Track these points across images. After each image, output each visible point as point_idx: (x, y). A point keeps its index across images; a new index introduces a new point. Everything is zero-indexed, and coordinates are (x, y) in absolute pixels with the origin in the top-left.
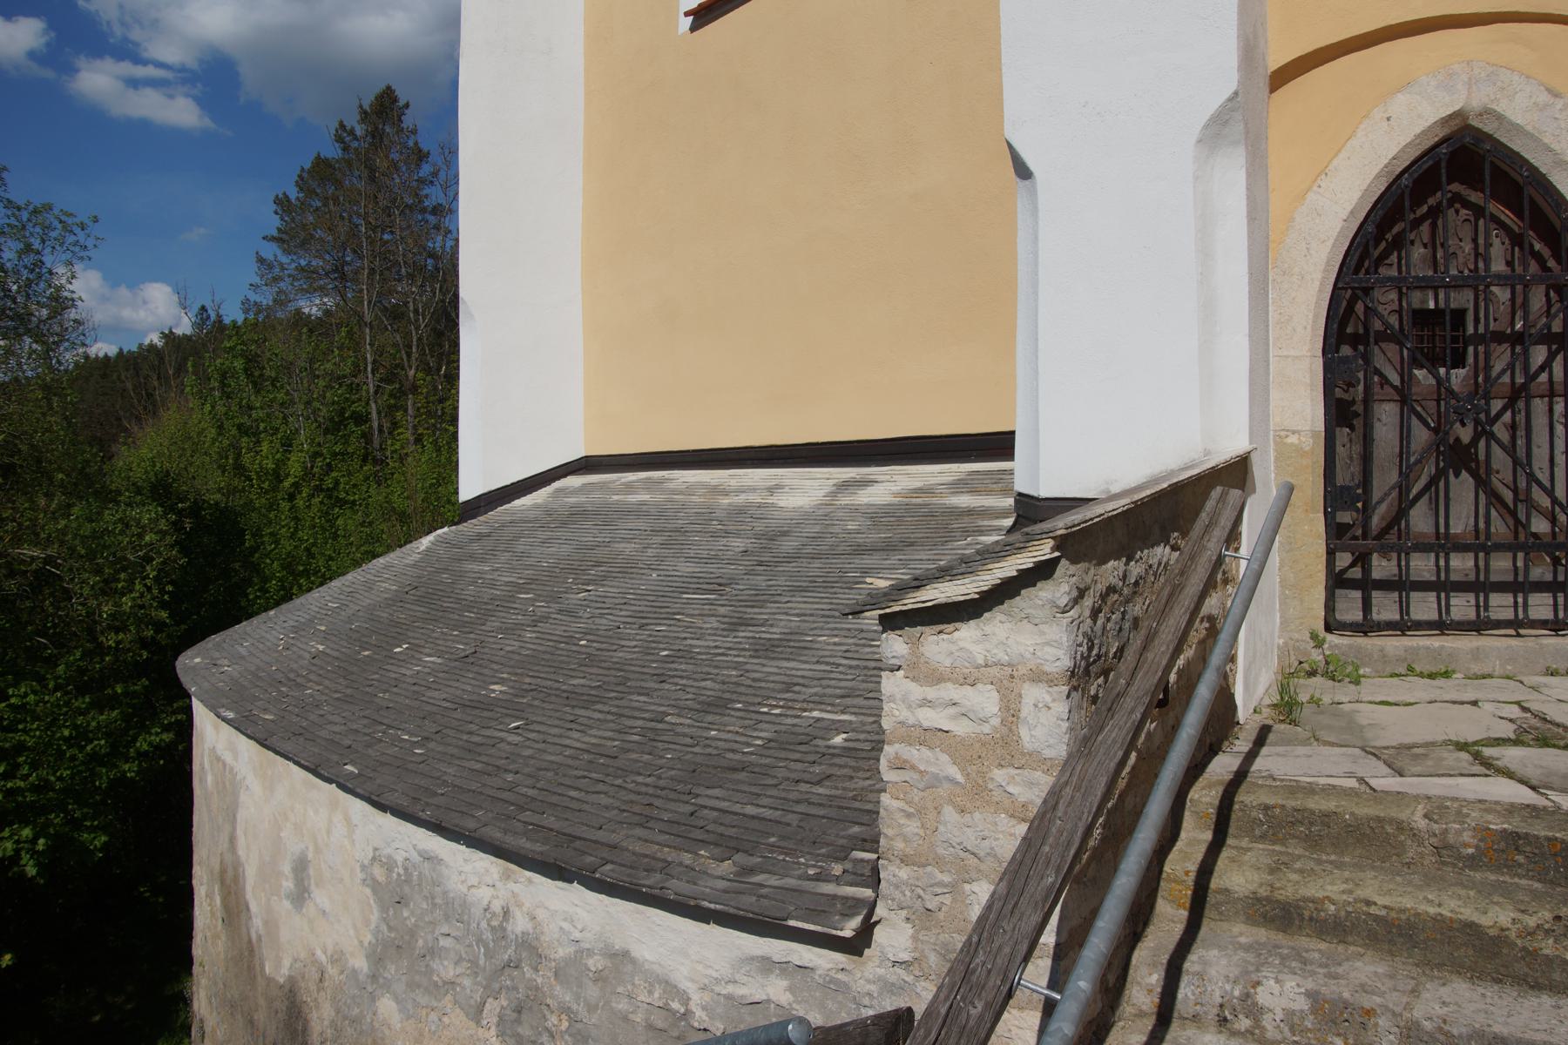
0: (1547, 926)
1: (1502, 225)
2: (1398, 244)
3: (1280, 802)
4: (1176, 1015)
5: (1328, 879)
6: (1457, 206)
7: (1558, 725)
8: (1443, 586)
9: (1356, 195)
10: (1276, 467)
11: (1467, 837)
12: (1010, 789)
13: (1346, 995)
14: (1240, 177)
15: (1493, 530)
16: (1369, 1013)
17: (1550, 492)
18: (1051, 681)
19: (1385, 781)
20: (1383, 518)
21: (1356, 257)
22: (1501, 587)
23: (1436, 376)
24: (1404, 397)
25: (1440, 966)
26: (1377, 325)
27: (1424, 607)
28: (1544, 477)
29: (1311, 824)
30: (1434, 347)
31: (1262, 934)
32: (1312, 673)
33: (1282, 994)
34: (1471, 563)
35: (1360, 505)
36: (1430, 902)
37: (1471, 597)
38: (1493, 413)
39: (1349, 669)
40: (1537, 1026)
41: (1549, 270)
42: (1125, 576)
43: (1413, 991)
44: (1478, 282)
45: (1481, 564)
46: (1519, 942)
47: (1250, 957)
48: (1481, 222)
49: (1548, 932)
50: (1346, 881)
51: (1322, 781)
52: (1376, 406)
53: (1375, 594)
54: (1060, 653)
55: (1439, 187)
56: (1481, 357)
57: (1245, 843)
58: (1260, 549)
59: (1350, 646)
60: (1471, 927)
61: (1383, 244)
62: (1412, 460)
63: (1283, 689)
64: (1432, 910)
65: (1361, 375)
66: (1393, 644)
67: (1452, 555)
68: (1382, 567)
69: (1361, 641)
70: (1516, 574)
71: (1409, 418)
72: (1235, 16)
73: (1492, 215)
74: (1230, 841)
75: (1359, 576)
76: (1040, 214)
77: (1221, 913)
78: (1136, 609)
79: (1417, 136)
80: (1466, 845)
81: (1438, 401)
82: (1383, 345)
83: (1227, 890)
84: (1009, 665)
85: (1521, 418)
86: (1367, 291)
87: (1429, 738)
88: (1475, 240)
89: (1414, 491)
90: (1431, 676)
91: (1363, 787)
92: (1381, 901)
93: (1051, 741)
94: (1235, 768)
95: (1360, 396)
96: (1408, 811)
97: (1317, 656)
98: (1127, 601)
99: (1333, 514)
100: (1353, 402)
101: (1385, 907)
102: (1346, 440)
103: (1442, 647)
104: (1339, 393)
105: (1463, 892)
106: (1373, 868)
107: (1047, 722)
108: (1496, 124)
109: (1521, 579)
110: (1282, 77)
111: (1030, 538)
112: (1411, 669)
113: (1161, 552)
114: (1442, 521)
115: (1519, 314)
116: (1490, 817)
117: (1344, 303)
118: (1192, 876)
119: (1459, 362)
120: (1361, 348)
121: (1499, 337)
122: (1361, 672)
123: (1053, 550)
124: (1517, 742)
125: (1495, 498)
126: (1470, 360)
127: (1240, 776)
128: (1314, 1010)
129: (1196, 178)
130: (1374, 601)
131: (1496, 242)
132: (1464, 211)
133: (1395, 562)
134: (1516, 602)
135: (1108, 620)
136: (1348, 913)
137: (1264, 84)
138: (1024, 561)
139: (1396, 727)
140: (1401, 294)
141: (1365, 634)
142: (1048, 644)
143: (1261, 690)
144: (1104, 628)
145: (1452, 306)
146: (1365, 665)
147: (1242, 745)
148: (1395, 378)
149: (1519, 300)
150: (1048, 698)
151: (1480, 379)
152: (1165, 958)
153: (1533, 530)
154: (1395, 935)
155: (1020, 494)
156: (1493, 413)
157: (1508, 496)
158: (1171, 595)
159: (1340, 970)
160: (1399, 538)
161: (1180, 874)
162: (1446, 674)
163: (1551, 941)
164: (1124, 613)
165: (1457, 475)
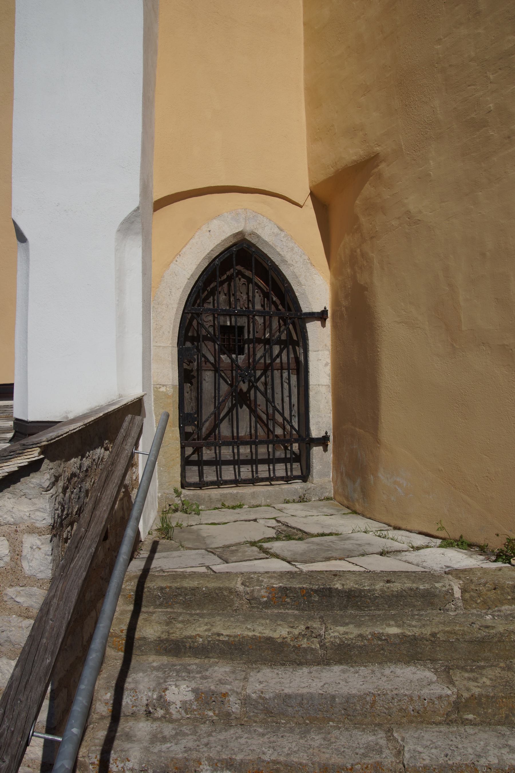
0: (303, 633)
1: (259, 288)
2: (212, 293)
3: (169, 585)
4: (122, 714)
5: (197, 624)
6: (240, 276)
7: (294, 528)
8: (237, 462)
9: (194, 267)
10: (155, 404)
11: (263, 592)
12: (18, 599)
13: (213, 687)
15: (258, 434)
16: (225, 695)
17: (282, 415)
18: (40, 533)
19: (220, 567)
20: (207, 429)
21: (194, 298)
22: (263, 462)
23: (231, 358)
24: (216, 369)
25: (256, 662)
26: (204, 332)
27: (228, 473)
28: (279, 408)
29: (186, 595)
30: (230, 344)
31: (165, 659)
32: (176, 511)
33: (179, 693)
34: (249, 450)
35: (196, 423)
36: (249, 629)
37: (249, 467)
38: (257, 377)
39: (194, 507)
40: (303, 685)
41: (280, 310)
42: (80, 467)
43: (245, 678)
44: (249, 314)
45: (254, 451)
46: (291, 643)
47: (160, 674)
48: (251, 285)
49: (304, 636)
50: (206, 624)
51: (189, 570)
52: (203, 372)
53: (205, 468)
54: (45, 515)
55: (232, 267)
56: (251, 350)
57: (151, 609)
58: (154, 449)
59: (194, 495)
60: (269, 639)
61: (206, 293)
62: (221, 399)
63: (163, 520)
64: (250, 634)
65: (196, 357)
66: (215, 493)
67: (240, 447)
68: (208, 454)
69: (199, 492)
70: (269, 455)
71: (219, 379)
73: (256, 283)
74: (143, 609)
75: (197, 459)
77: (142, 651)
78: (87, 485)
79: (223, 241)
80: (263, 597)
81: (232, 371)
82: (206, 342)
83: (144, 638)
84: (14, 524)
85: (269, 379)
86: (199, 315)
87: (237, 541)
88: (248, 294)
89: (222, 416)
90: (233, 508)
91: (209, 571)
92: (225, 633)
93: (42, 568)
94: (142, 567)
95: (195, 368)
96: (234, 583)
97: (178, 501)
98: (82, 481)
99: (183, 427)
100: (192, 371)
101: (227, 636)
102: (189, 390)
103: (238, 493)
104: (185, 366)
105: (263, 622)
106: (219, 615)
107: (39, 557)
108: (257, 240)
109: (271, 457)
110: (160, 204)
111: (26, 447)
112: (223, 505)
113: (100, 451)
114: (235, 430)
115: (267, 330)
116: (273, 581)
117: (188, 321)
118: (125, 632)
119: (241, 352)
120: (196, 343)
121: (259, 341)
122: (200, 508)
123: (40, 454)
124: (277, 539)
125: (259, 418)
126: (246, 351)
127: (146, 571)
128: (197, 699)
130: (204, 471)
131: (257, 295)
132: (242, 280)
133: (213, 451)
134: (269, 469)
135: (72, 492)
136: (209, 641)
138: (22, 461)
139: (223, 535)
140: (214, 318)
141: (201, 488)
142: (37, 510)
143: (151, 521)
144: (70, 498)
145: (238, 325)
146: (201, 504)
147: (144, 554)
148: (212, 359)
149: (267, 323)
150: (39, 543)
151: (251, 361)
152: (113, 683)
153: (276, 434)
154: (235, 650)
155: (17, 419)
156: (257, 377)
157: (264, 417)
158: (107, 477)
159: (207, 673)
160: (215, 439)
161: (118, 632)
162: (240, 506)
163: (305, 640)
164: (80, 488)
165: (241, 407)
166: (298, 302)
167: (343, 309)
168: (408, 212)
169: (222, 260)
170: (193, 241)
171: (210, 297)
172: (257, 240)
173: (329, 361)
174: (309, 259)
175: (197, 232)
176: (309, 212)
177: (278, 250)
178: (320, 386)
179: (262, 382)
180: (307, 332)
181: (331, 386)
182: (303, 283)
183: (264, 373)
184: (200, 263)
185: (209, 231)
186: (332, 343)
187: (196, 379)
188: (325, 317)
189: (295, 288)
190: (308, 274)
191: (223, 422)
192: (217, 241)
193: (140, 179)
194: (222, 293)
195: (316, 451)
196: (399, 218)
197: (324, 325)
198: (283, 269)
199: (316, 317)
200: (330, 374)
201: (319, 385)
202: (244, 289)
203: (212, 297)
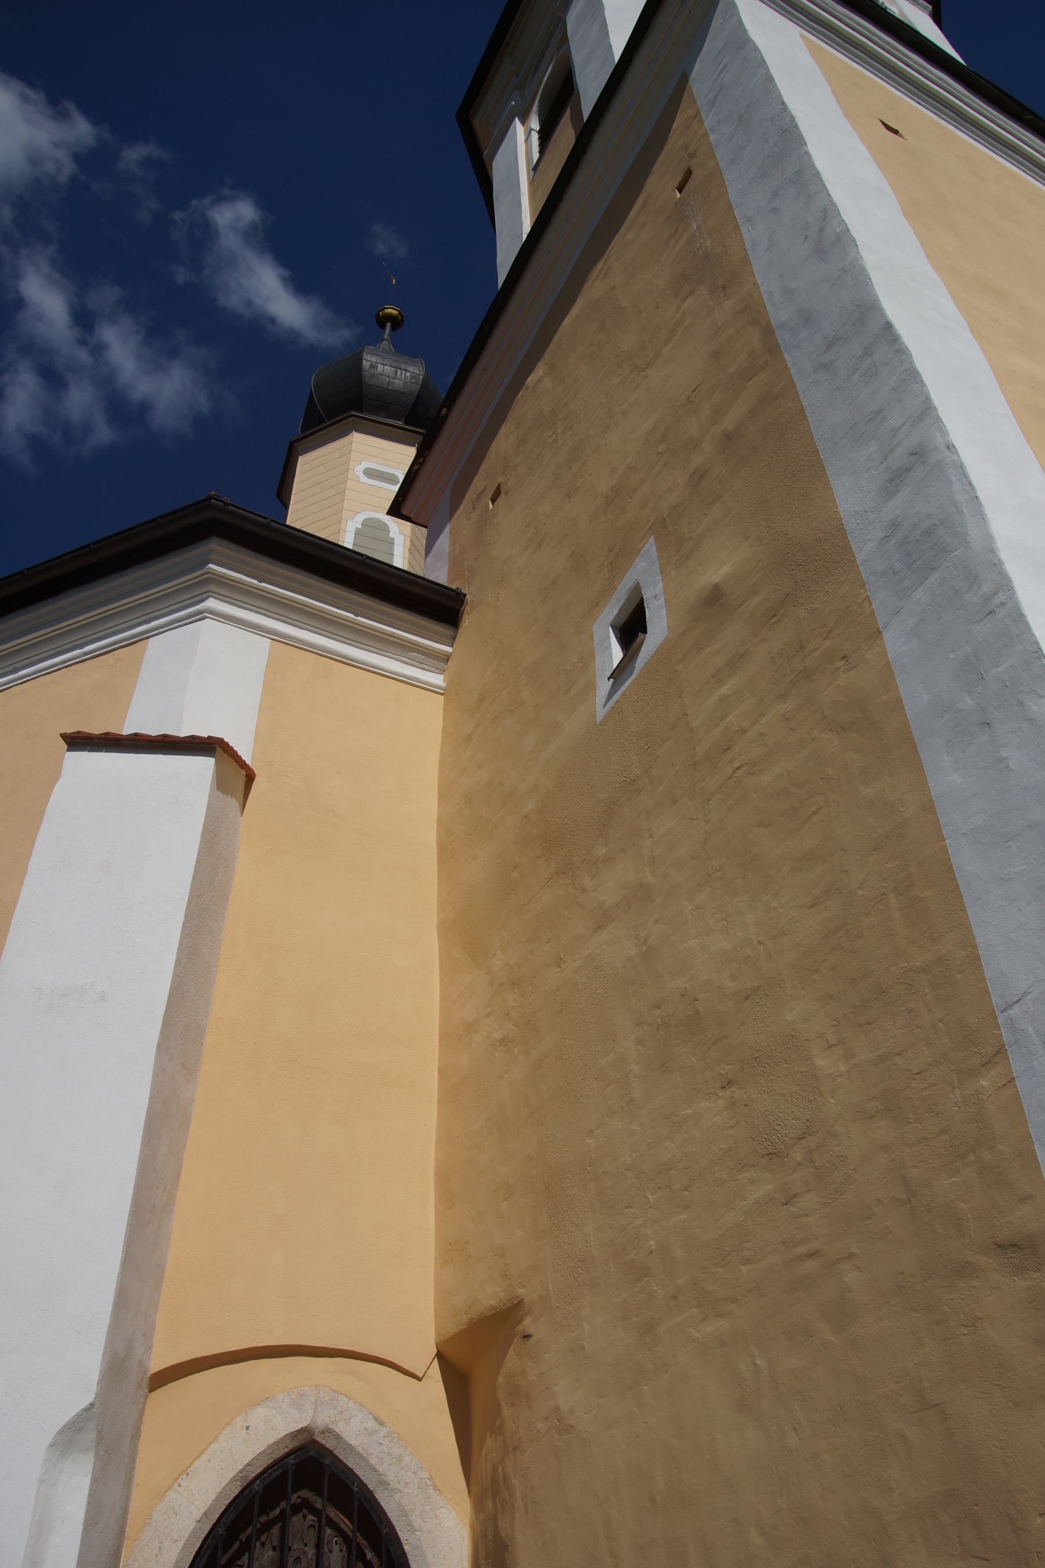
1: (340, 1532)
6: (305, 1511)
9: (211, 1497)
14: (86, 1482)
72: (104, 1336)
76: (254, 787)
79: (270, 1446)
108: (335, 1442)
129: (42, 1482)
132: (310, 1517)
137: (145, 1383)
168: (557, 1409)
169: (266, 1482)
170: (215, 1446)
171: (243, 1554)
172: (335, 1442)
174: (430, 1478)
175: (223, 1429)
176: (435, 1387)
177: (372, 1462)
182: (417, 1527)
184: (224, 1489)
185: (247, 1428)
189: (403, 1535)
190: (428, 1508)
192: (259, 1447)
193: (104, 1353)
194: (268, 1545)
196: (546, 1419)
198: (381, 1496)
202: (311, 1537)
203: (247, 1555)
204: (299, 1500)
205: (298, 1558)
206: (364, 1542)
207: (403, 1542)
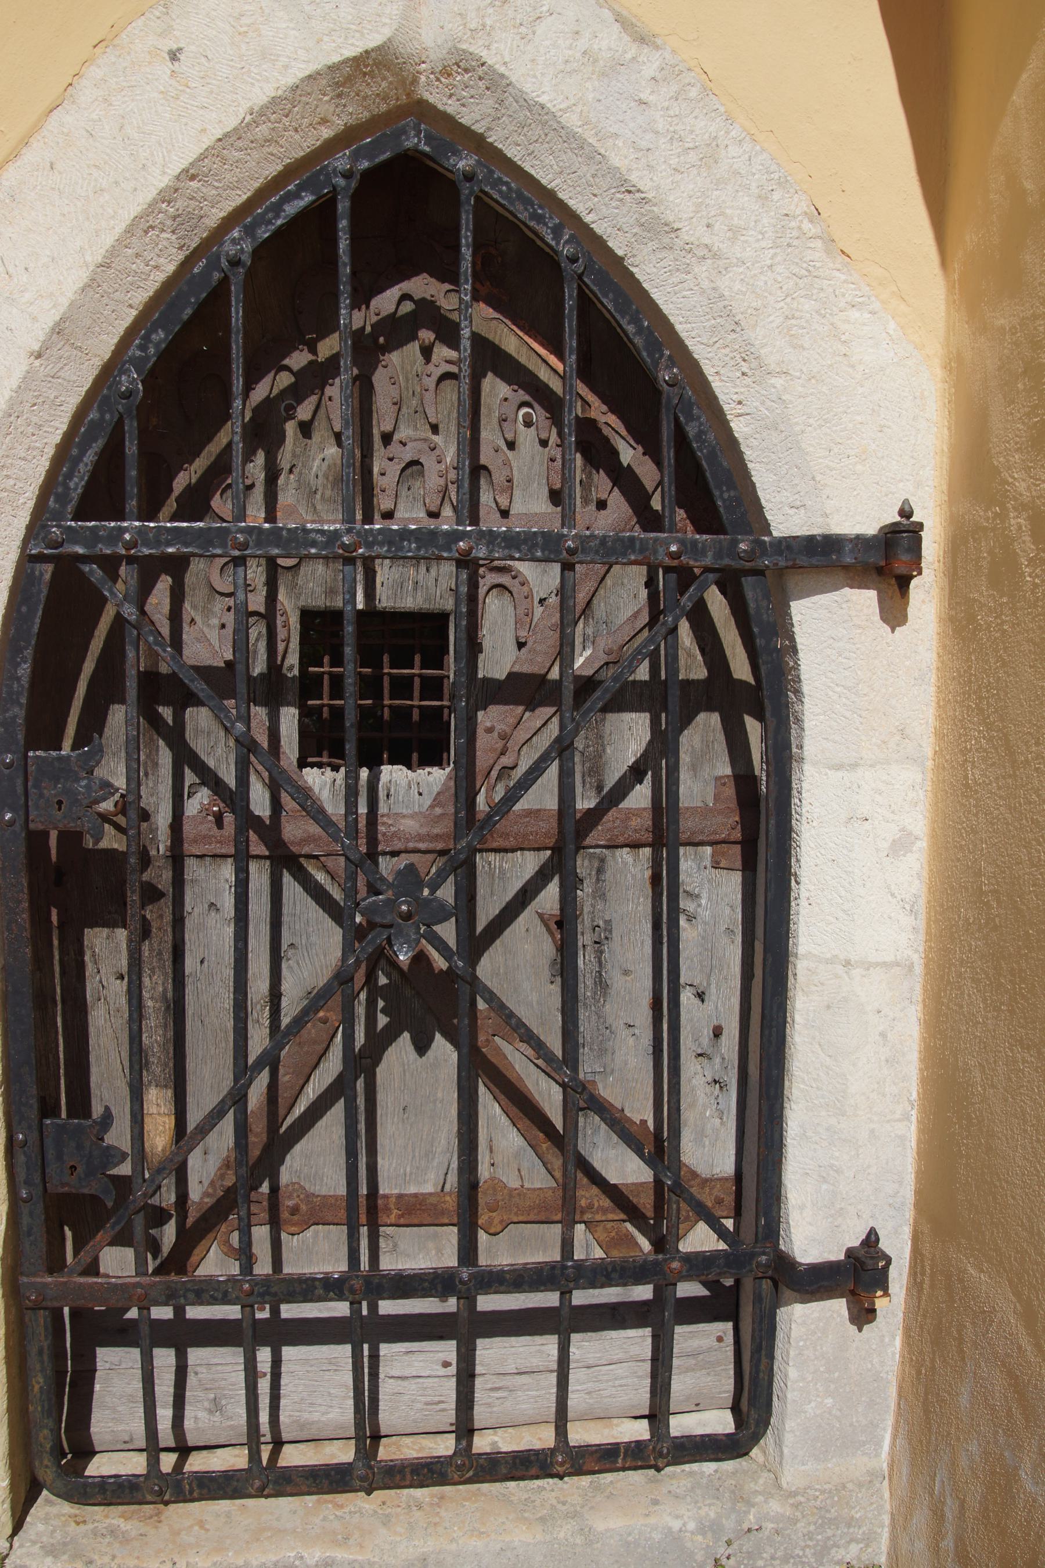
6: (426, 335)
17: (659, 1146)
28: (631, 1091)
108: (489, 103)
131: (527, 438)
166: (746, 475)
167: (1017, 521)
169: (264, 233)
172: (489, 103)
173: (918, 822)
177: (616, 161)
178: (856, 972)
179: (541, 916)
180: (794, 650)
181: (919, 969)
183: (560, 864)
184: (113, 252)
185: (174, 56)
186: (939, 717)
187: (166, 906)
188: (900, 569)
189: (725, 389)
191: (322, 1123)
195: (809, 1328)
197: (894, 613)
199: (846, 568)
200: (922, 902)
201: (847, 963)
202: (446, 406)
204: (408, 307)
205: (415, 463)
206: (612, 419)
207: (729, 409)
